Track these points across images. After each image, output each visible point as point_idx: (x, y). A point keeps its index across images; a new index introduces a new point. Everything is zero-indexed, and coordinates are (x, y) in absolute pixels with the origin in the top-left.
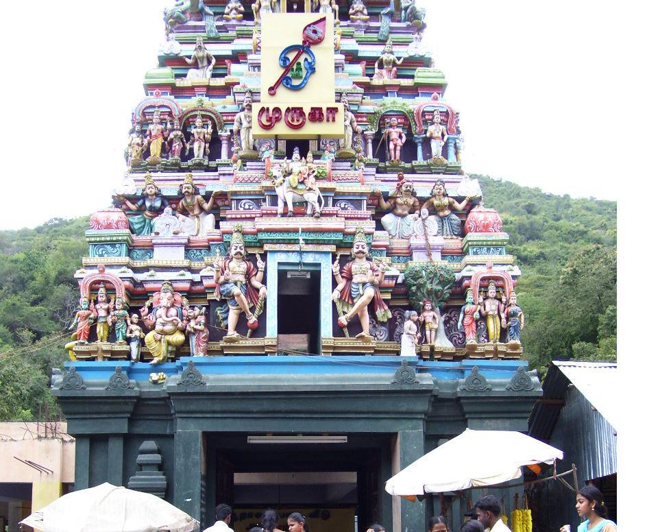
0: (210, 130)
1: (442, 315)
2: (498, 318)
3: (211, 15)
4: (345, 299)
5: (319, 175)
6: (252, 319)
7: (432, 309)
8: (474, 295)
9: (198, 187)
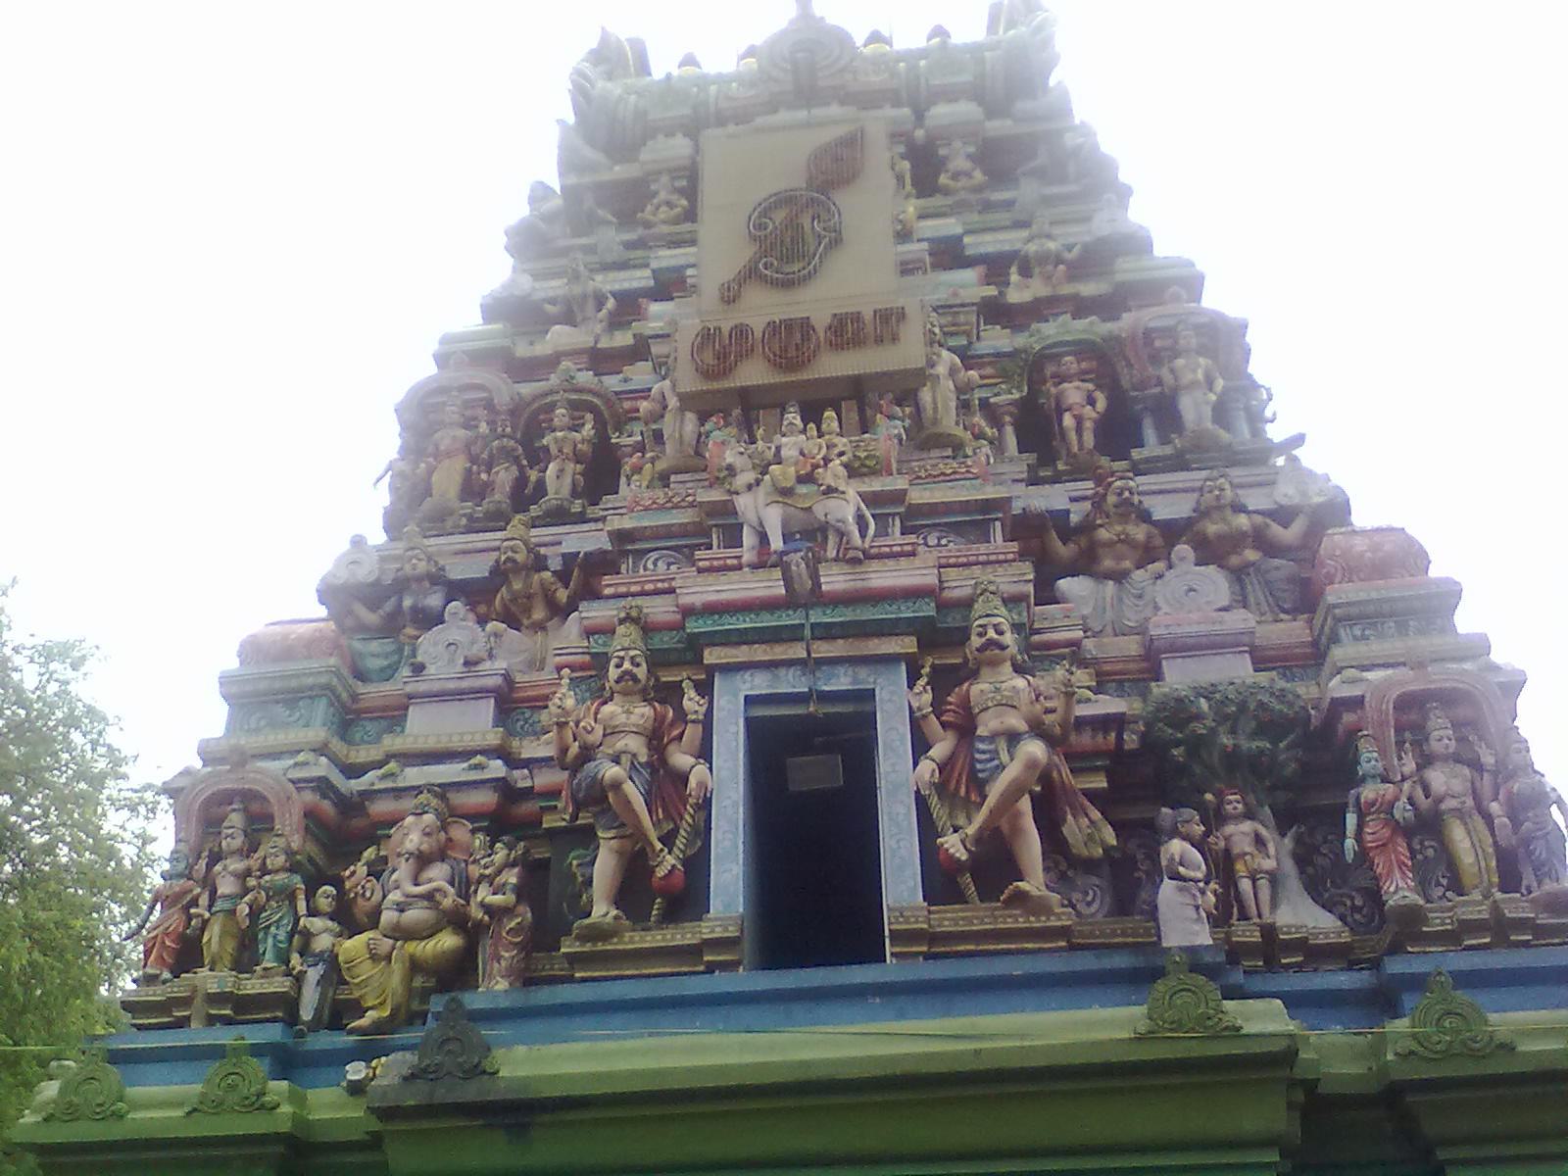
0: (588, 430)
1: (1283, 835)
2: (1479, 822)
3: (609, 223)
4: (958, 788)
5: (857, 464)
6: (668, 862)
7: (1249, 815)
8: (1383, 753)
9: (543, 551)
